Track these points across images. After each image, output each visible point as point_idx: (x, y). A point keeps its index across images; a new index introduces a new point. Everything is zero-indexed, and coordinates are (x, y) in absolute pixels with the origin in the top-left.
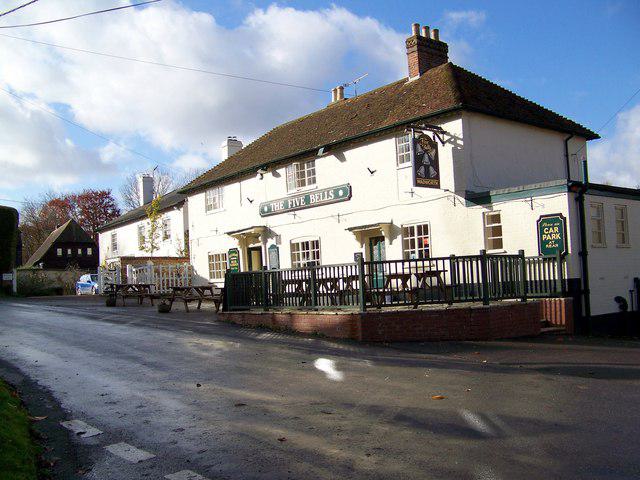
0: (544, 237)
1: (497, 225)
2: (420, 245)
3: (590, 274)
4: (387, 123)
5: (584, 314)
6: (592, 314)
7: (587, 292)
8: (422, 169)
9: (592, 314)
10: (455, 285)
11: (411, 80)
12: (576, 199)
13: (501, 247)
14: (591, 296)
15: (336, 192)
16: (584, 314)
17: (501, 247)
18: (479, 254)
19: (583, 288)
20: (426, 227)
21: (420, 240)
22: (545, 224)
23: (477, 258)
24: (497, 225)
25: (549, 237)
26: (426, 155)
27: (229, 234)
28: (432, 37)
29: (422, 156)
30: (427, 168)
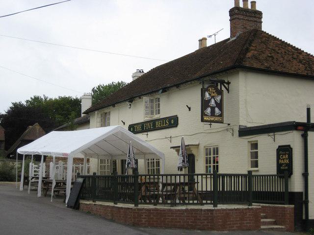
0: (280, 161)
1: (256, 151)
2: (214, 163)
3: (310, 192)
4: (197, 76)
5: (304, 217)
6: (310, 218)
7: (306, 202)
8: (209, 110)
9: (310, 218)
10: (230, 192)
11: (231, 40)
12: (303, 136)
13: (258, 167)
14: (310, 205)
15: (170, 121)
16: (304, 217)
17: (258, 167)
18: (247, 173)
19: (304, 199)
20: (217, 149)
21: (214, 157)
22: (281, 152)
23: (245, 176)
24: (256, 151)
25: (282, 162)
26: (213, 100)
27: (308, 110)
28: (250, 7)
29: (209, 101)
30: (213, 109)
